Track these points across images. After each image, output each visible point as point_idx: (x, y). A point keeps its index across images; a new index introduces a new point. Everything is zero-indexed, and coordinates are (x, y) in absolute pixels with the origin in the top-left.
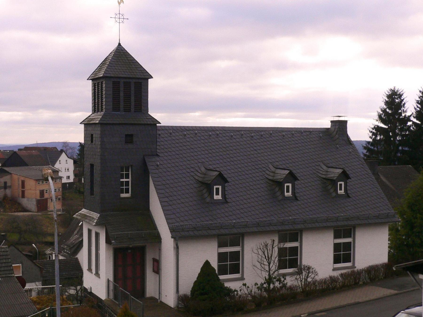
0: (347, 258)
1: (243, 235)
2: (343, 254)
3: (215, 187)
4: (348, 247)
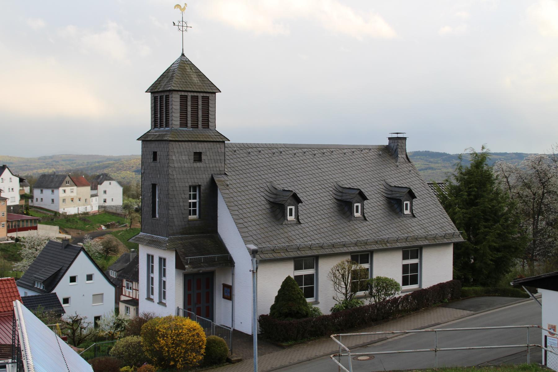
0: (414, 280)
1: (317, 258)
2: (411, 274)
3: (289, 208)
4: (415, 268)
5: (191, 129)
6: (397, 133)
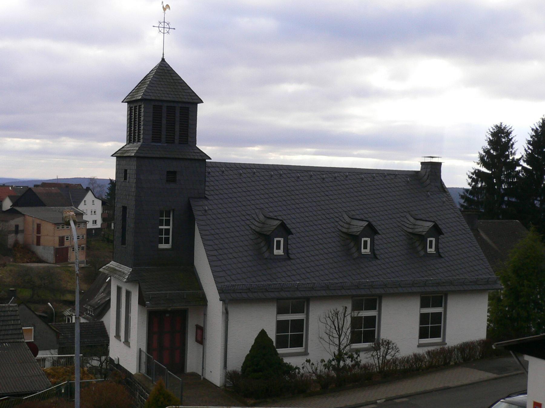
0: (436, 332)
4: (438, 318)
5: (166, 145)
6: (432, 157)
